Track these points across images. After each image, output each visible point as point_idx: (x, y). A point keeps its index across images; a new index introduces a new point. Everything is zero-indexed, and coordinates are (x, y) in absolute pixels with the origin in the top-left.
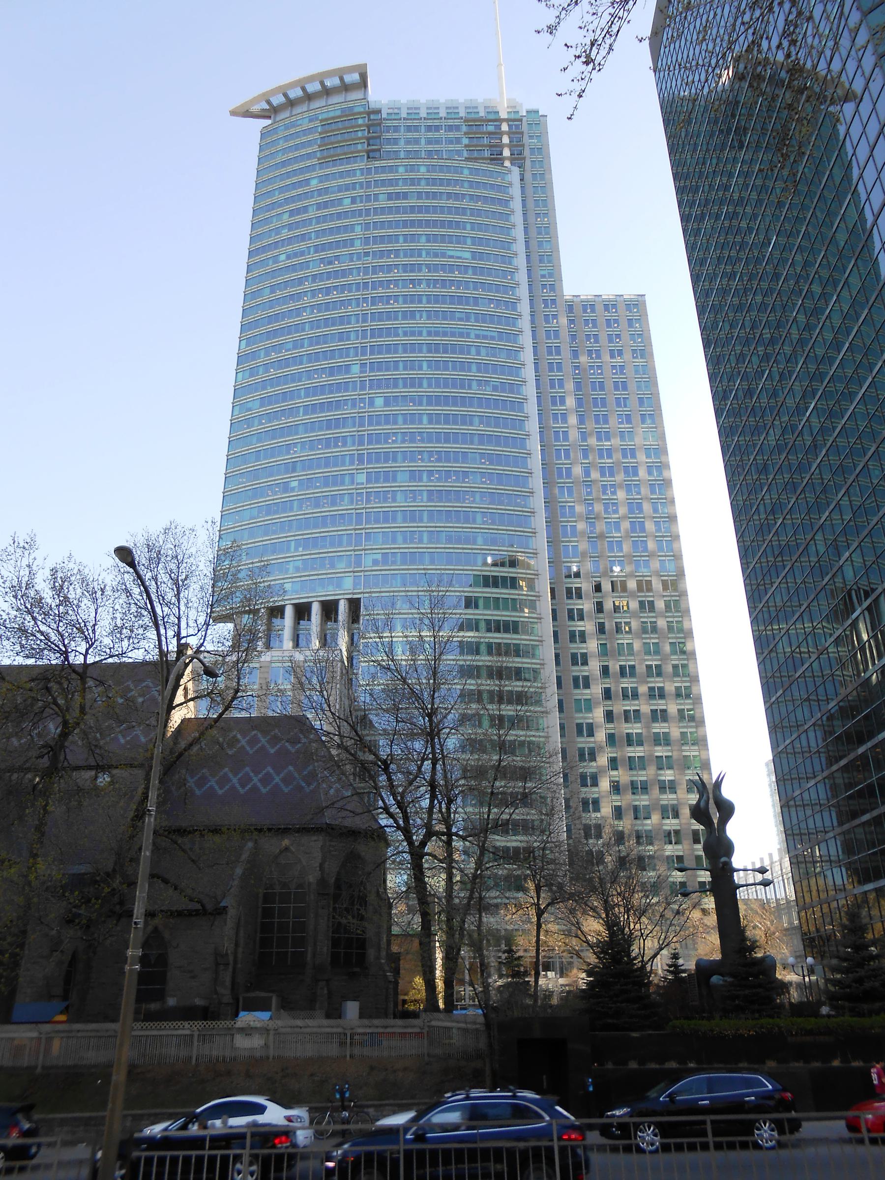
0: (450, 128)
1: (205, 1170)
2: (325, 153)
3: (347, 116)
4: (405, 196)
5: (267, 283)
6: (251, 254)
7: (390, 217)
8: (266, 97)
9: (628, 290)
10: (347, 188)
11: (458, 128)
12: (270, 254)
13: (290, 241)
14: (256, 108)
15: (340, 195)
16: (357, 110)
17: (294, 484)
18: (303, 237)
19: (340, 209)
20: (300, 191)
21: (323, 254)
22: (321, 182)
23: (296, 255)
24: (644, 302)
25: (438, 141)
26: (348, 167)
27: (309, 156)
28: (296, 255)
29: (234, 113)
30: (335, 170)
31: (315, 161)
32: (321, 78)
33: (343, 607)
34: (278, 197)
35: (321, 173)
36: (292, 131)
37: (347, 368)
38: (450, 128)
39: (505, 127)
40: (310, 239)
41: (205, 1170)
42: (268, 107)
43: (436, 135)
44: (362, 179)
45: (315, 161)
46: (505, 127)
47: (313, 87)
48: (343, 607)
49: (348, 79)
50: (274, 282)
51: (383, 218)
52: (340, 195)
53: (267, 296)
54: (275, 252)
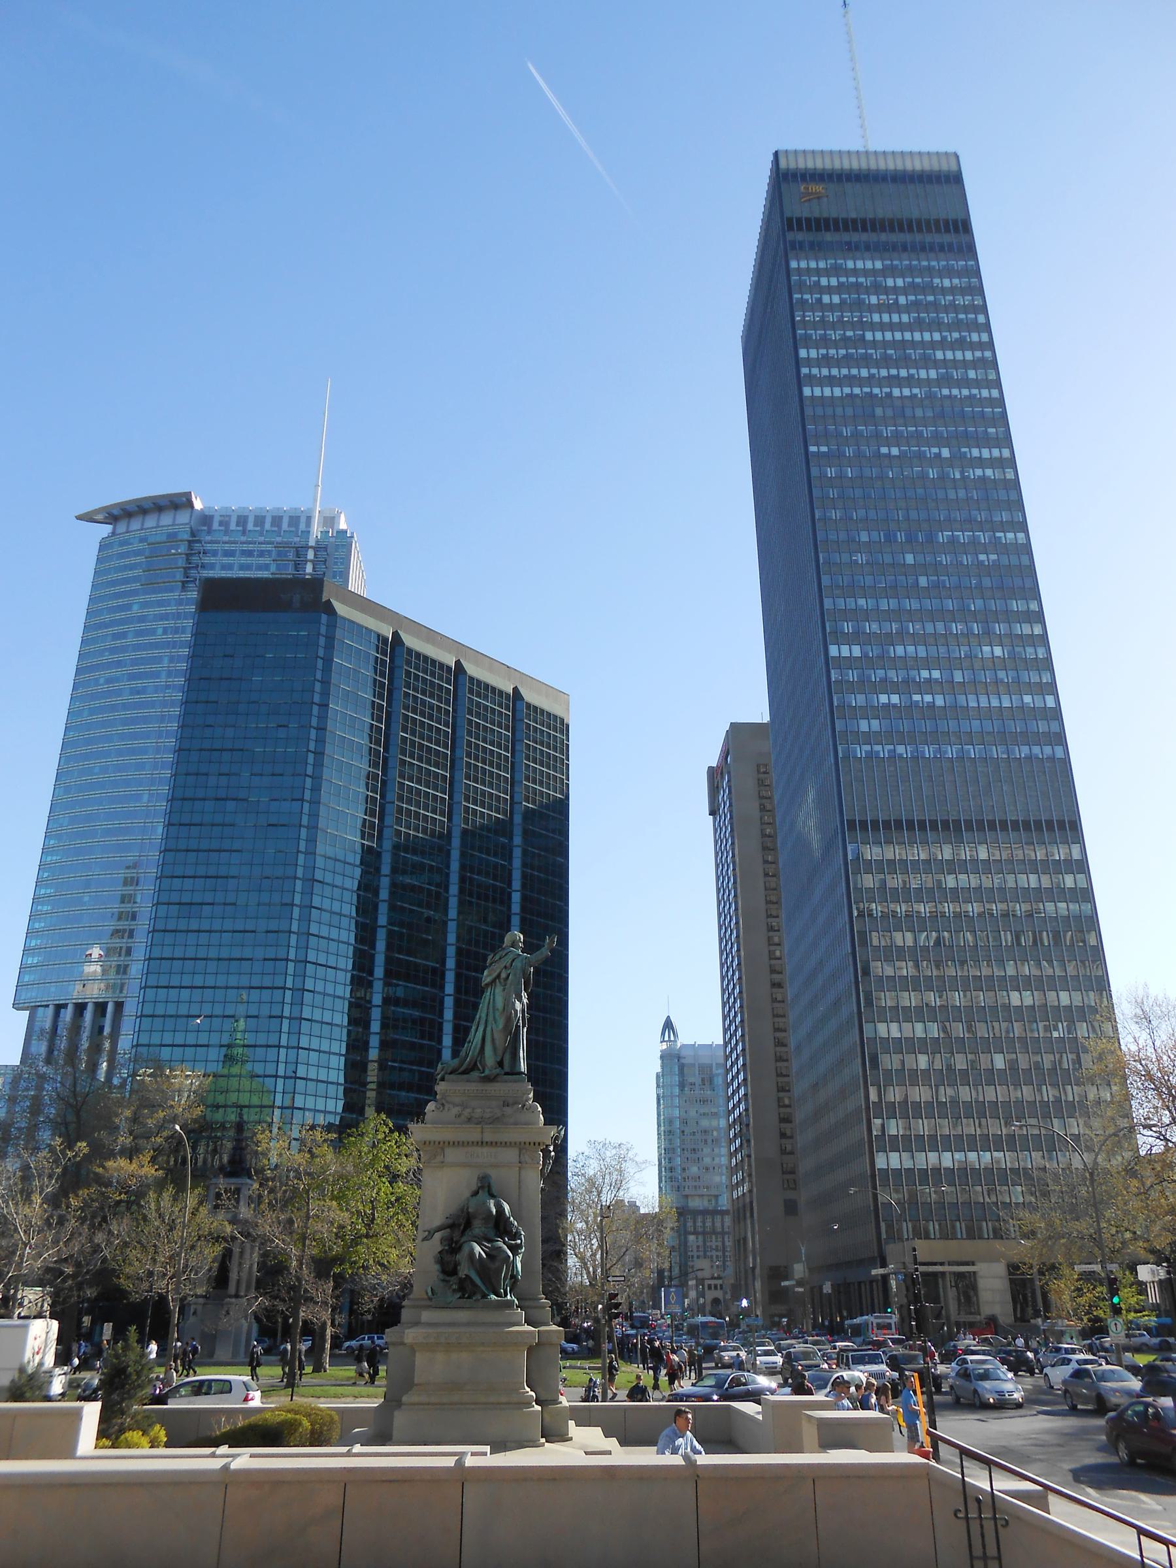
6: (79, 671)
13: (109, 665)
14: (100, 517)
17: (86, 899)
18: (119, 664)
29: (79, 518)
31: (136, 586)
33: (110, 1008)
34: (107, 618)
35: (142, 598)
37: (138, 797)
39: (311, 555)
45: (136, 586)
46: (311, 555)
48: (110, 1008)
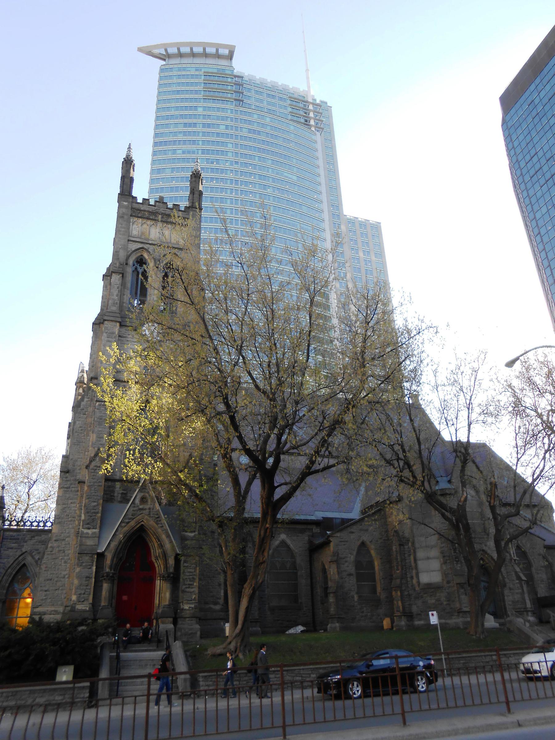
0: (281, 99)
1: (371, 686)
2: (207, 93)
3: (221, 74)
4: (259, 133)
5: (169, 166)
7: (250, 144)
8: (165, 46)
9: (373, 218)
10: (223, 118)
11: (285, 100)
12: (170, 147)
14: (156, 51)
15: (219, 122)
16: (227, 72)
19: (218, 131)
20: (191, 112)
21: (208, 156)
22: (204, 110)
23: (189, 152)
24: (380, 227)
25: (274, 105)
26: (223, 106)
27: (196, 92)
28: (189, 152)
29: (140, 50)
30: (214, 105)
32: (191, 45)
35: (205, 105)
36: (184, 73)
38: (281, 99)
40: (198, 144)
41: (371, 686)
42: (164, 53)
43: (273, 101)
44: (232, 116)
47: (185, 50)
49: (209, 50)
50: (173, 165)
51: (246, 143)
52: (219, 122)
53: (168, 174)
54: (175, 147)
